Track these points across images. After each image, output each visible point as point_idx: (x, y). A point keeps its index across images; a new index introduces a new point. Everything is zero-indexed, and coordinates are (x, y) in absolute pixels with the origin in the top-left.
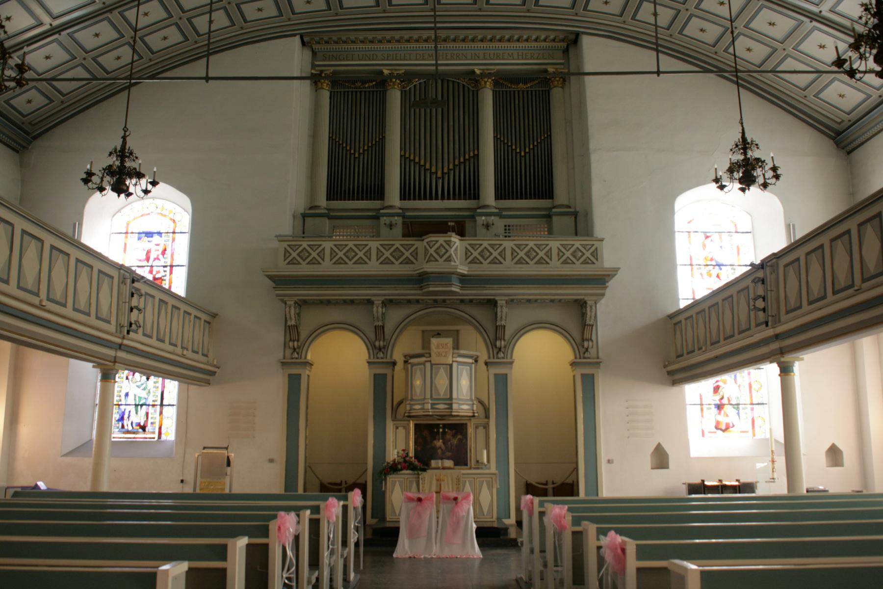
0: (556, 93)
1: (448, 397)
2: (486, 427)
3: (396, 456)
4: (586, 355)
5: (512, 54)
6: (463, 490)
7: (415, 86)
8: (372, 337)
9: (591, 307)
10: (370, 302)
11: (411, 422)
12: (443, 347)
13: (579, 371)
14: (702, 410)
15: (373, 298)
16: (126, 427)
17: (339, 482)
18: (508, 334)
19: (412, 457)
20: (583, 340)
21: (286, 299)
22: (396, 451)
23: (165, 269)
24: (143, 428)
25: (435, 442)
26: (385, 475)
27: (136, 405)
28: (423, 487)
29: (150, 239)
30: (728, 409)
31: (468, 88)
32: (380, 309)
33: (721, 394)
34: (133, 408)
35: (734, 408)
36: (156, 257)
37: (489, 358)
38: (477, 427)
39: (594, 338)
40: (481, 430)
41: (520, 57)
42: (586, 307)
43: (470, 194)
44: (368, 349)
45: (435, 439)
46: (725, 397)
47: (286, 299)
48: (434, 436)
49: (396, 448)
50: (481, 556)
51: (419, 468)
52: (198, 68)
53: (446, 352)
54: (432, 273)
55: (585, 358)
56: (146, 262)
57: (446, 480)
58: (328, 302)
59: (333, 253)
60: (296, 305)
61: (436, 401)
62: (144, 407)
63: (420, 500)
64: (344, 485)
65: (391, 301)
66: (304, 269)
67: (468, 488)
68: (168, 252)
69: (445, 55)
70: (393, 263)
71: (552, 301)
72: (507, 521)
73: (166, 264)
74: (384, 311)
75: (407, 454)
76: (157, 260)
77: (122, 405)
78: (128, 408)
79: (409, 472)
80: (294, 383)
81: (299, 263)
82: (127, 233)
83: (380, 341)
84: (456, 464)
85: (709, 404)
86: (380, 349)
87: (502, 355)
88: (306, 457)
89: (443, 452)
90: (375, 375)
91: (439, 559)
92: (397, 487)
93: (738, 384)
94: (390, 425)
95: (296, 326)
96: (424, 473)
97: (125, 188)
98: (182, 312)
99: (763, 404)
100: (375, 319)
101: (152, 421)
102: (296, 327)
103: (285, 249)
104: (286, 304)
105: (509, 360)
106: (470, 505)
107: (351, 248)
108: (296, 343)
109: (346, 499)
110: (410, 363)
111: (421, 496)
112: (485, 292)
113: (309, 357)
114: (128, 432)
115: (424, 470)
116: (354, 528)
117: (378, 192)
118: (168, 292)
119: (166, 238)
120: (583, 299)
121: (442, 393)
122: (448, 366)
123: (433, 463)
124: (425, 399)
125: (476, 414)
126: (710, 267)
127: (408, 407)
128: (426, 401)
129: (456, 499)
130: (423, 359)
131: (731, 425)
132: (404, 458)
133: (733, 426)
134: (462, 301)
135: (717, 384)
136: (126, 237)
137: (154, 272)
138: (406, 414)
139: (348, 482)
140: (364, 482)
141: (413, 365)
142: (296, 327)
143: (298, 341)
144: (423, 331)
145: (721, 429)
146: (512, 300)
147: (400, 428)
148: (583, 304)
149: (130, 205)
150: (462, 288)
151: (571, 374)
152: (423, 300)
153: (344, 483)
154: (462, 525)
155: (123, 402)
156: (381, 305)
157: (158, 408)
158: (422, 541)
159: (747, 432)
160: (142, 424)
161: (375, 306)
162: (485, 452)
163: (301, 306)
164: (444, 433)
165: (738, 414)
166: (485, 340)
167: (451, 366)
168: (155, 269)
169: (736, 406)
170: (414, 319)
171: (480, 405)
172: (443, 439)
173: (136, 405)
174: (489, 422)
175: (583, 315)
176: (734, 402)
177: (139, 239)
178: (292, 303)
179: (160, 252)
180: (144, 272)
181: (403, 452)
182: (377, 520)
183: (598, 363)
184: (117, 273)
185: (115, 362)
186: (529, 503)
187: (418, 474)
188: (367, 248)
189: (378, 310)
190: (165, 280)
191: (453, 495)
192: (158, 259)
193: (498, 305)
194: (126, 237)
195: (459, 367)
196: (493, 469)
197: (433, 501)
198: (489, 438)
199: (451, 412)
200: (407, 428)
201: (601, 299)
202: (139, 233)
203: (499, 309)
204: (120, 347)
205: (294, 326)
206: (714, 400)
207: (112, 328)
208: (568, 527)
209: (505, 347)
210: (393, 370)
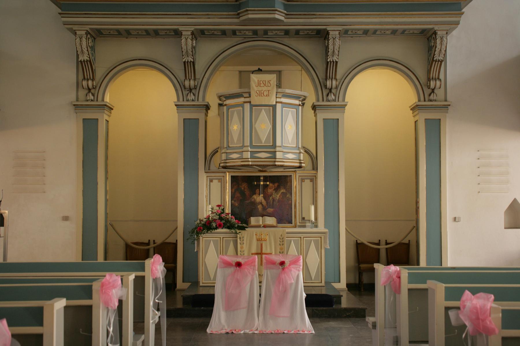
2: (313, 180)
3: (210, 212)
4: (431, 97)
6: (287, 253)
8: (181, 75)
9: (442, 38)
10: (177, 34)
12: (265, 85)
13: (422, 117)
15: (181, 28)
17: (147, 241)
18: (340, 72)
19: (228, 214)
20: (429, 80)
21: (75, 28)
22: (210, 206)
25: (255, 197)
26: (198, 234)
28: (242, 248)
32: (189, 41)
37: (318, 100)
38: (302, 180)
39: (442, 77)
40: (307, 184)
42: (435, 39)
44: (176, 90)
45: (255, 193)
47: (75, 28)
49: (210, 204)
50: (313, 332)
55: (431, 101)
57: (268, 240)
60: (89, 36)
61: (256, 148)
63: (239, 264)
64: (152, 245)
65: (202, 32)
67: (293, 250)
71: (394, 32)
72: (336, 286)
74: (194, 45)
75: (223, 210)
83: (190, 80)
84: (280, 221)
86: (190, 90)
87: (333, 97)
88: (106, 214)
89: (264, 209)
91: (262, 335)
92: (212, 246)
94: (203, 178)
95: (90, 61)
96: (243, 232)
100: (184, 53)
102: (90, 62)
104: (75, 34)
106: (299, 271)
108: (90, 82)
109: (142, 268)
110: (226, 105)
111: (240, 260)
112: (314, 20)
113: (107, 99)
115: (243, 228)
116: (154, 306)
120: (433, 28)
121: (264, 139)
122: (271, 108)
123: (253, 220)
124: (243, 146)
125: (303, 165)
127: (224, 156)
128: (245, 149)
129: (282, 263)
130: (242, 100)
132: (219, 215)
134: (287, 32)
138: (222, 165)
139: (156, 242)
140: (175, 242)
141: (229, 107)
142: (90, 62)
143: (93, 80)
144: (240, 72)
146: (346, 32)
147: (214, 181)
148: (431, 36)
151: (413, 120)
152: (240, 30)
153: (152, 242)
154: (290, 295)
156: (190, 37)
158: (242, 314)
161: (183, 37)
162: (313, 208)
163: (95, 39)
164: (266, 186)
166: (313, 80)
167: (274, 107)
170: (229, 55)
171: (306, 154)
172: (264, 193)
174: (317, 173)
175: (430, 49)
178: (84, 33)
181: (218, 208)
182: (189, 284)
183: (446, 107)
186: (394, 277)
189: (187, 42)
191: (278, 259)
193: (330, 36)
196: (321, 228)
197: (254, 266)
198: (316, 192)
199: (275, 162)
200: (222, 181)
201: (454, 28)
203: (331, 42)
205: (87, 61)
208: (497, 331)
209: (336, 88)
210: (206, 115)
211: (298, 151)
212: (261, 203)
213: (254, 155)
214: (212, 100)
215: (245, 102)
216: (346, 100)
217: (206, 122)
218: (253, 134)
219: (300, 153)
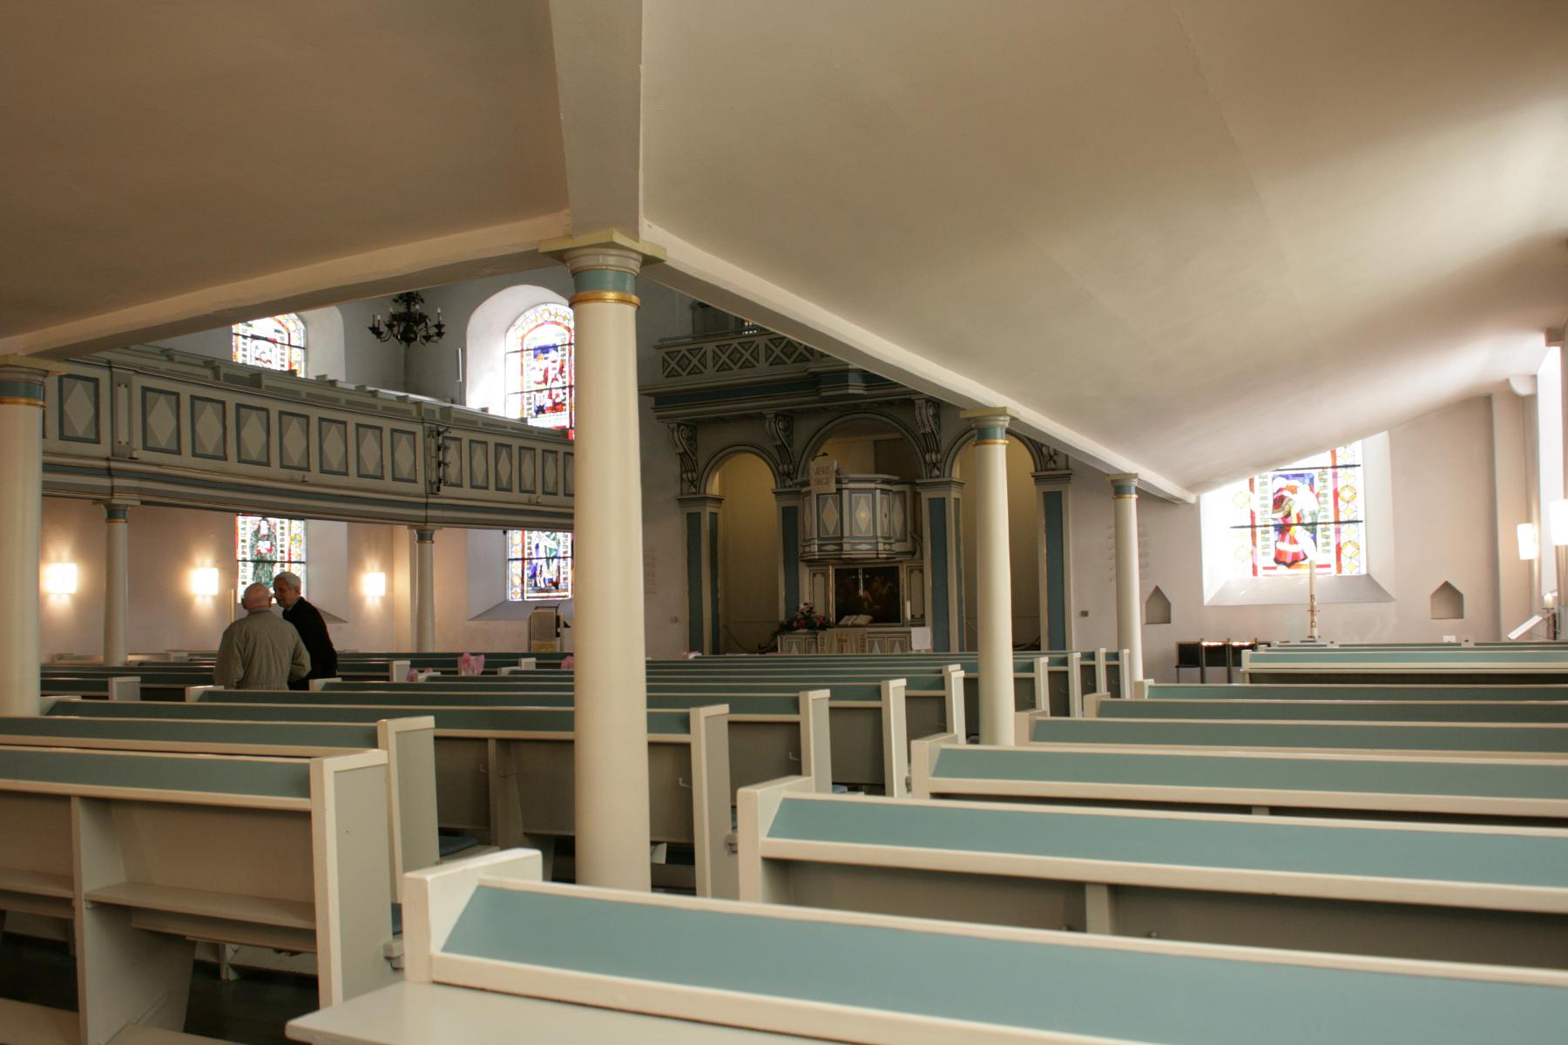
1: (839, 535)
10: (761, 417)
11: (830, 567)
14: (1254, 535)
15: (764, 411)
16: (539, 585)
24: (556, 585)
27: (548, 559)
29: (546, 355)
30: (1297, 532)
33: (1287, 508)
34: (543, 562)
35: (1307, 530)
36: (553, 376)
38: (911, 571)
46: (1292, 513)
51: (818, 624)
53: (828, 478)
54: (822, 373)
58: (724, 420)
59: (716, 357)
62: (555, 560)
66: (685, 382)
70: (784, 363)
76: (555, 382)
77: (533, 559)
78: (541, 562)
79: (806, 631)
81: (731, 369)
82: (522, 350)
85: (1265, 526)
90: (783, 508)
93: (1316, 493)
97: (413, 336)
99: (1357, 522)
101: (565, 576)
103: (663, 358)
107: (735, 348)
114: (542, 590)
119: (562, 353)
121: (831, 529)
130: (872, 486)
131: (1302, 557)
133: (1305, 557)
135: (1280, 494)
136: (522, 356)
137: (554, 396)
144: (875, 442)
145: (1284, 563)
147: (817, 575)
149: (522, 316)
150: (867, 388)
155: (534, 556)
157: (1258, 523)
159: (1328, 566)
160: (554, 580)
165: (1314, 539)
168: (554, 392)
169: (1310, 527)
173: (548, 559)
176: (1308, 520)
177: (535, 356)
178: (675, 425)
179: (558, 370)
184: (421, 427)
185: (426, 522)
187: (817, 634)
190: (565, 405)
192: (556, 379)
194: (522, 356)
195: (853, 495)
200: (825, 575)
202: (535, 349)
204: (426, 506)
206: (1274, 519)
211: (875, 541)
212: (867, 599)
215: (876, 489)
219: (877, 543)
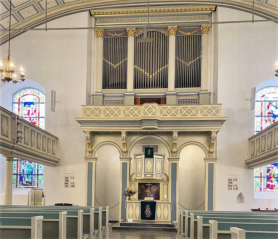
0: (204, 37)
5: (185, 17)
7: (141, 34)
16: (24, 183)
23: (36, 119)
31: (165, 35)
37: (170, 156)
41: (189, 19)
43: (164, 86)
48: (146, 187)
52: (43, 26)
56: (28, 115)
68: (37, 112)
69: (154, 19)
73: (36, 117)
80: (90, 165)
86: (125, 152)
98: (51, 140)
105: (177, 157)
113: (96, 156)
117: (124, 85)
118: (38, 128)
126: (270, 117)
137: (32, 120)
168: (32, 119)
180: (27, 120)
188: (119, 109)
204: (13, 148)
207: (10, 139)
210: (130, 161)
213: (123, 220)
214: (132, 156)
216: (180, 157)
217: (130, 164)
218: (146, 167)
